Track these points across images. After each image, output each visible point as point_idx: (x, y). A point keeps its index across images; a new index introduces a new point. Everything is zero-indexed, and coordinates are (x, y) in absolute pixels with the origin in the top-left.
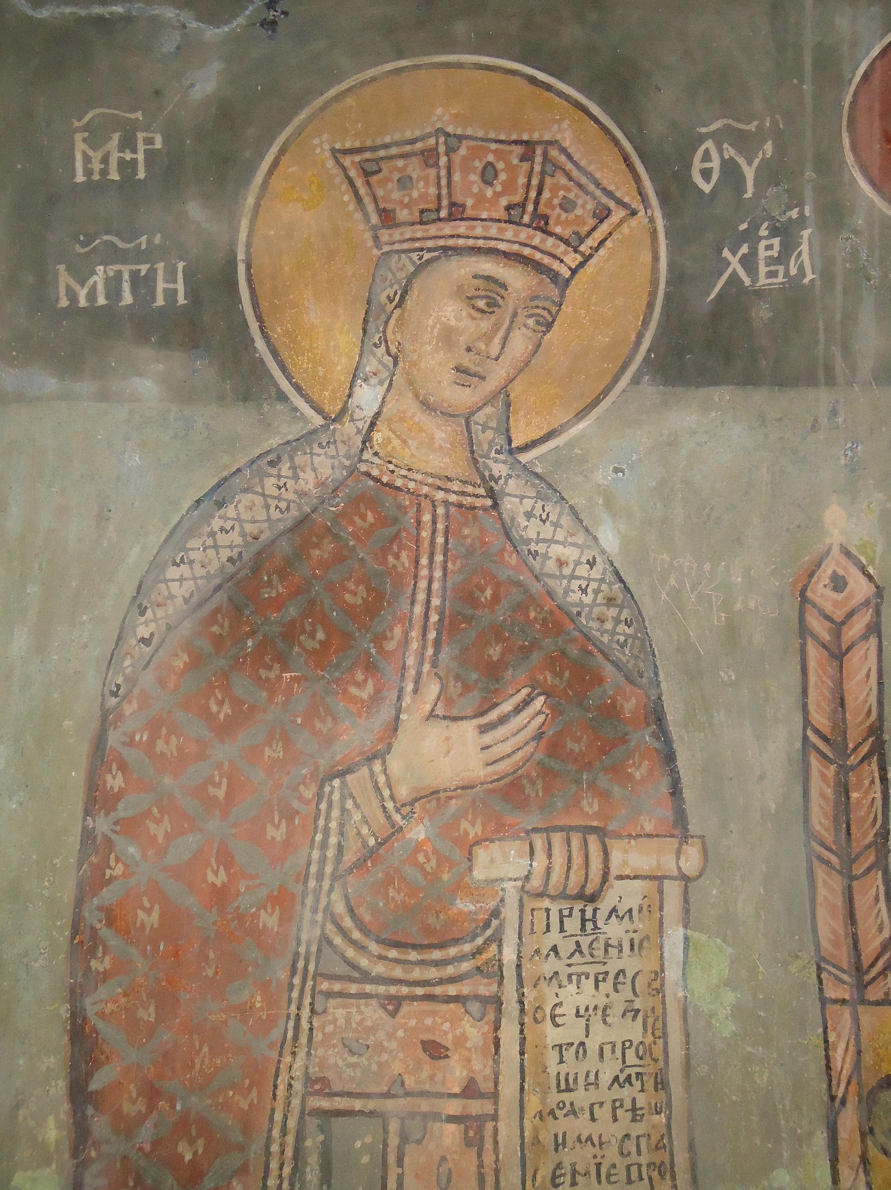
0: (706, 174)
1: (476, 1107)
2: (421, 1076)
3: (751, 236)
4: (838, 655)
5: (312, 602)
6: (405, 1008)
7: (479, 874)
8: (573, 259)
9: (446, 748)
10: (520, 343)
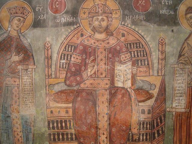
0: (37, 10)
1: (18, 86)
2: (14, 83)
3: (41, 15)
4: (48, 50)
5: (5, 46)
6: (13, 78)
7: (18, 68)
8: (26, 17)
9: (16, 58)
10: (22, 24)
